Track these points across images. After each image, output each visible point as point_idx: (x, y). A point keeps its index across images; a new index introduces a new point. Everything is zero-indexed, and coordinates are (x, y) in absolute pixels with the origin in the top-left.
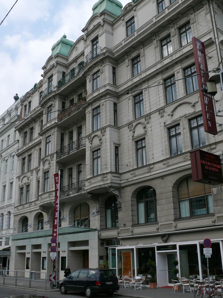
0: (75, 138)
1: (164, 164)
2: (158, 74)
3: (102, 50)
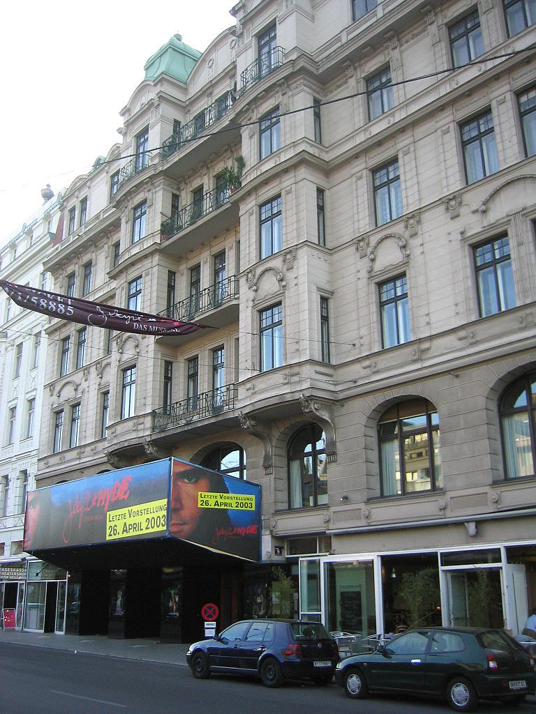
0: (206, 281)
1: (460, 339)
2: (442, 108)
3: (285, 55)
